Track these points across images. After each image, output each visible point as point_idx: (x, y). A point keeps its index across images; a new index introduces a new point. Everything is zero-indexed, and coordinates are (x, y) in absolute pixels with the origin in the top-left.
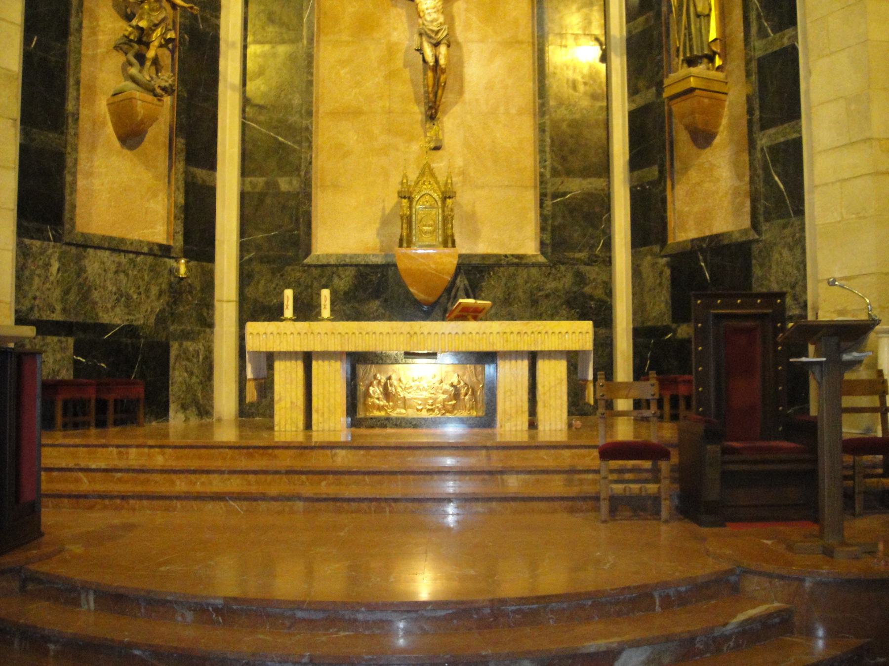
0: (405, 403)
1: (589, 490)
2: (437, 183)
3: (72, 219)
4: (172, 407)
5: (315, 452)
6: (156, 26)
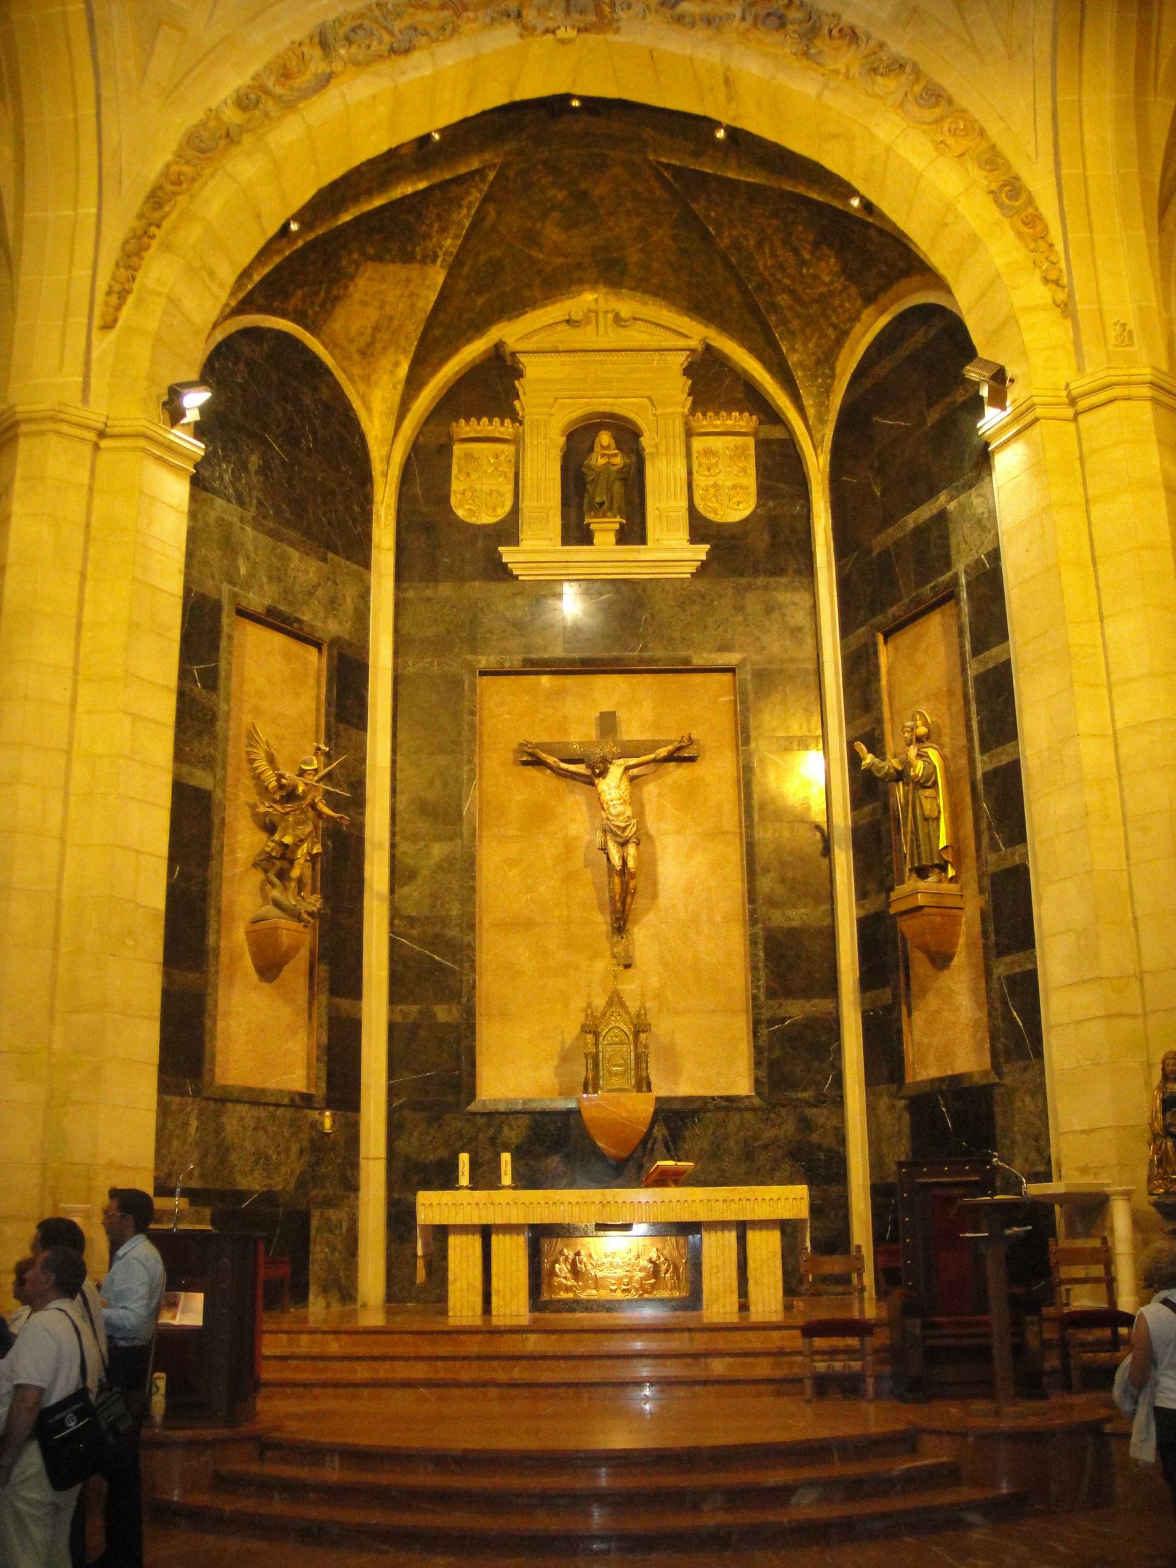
0: (597, 1283)
1: (797, 1371)
2: (628, 1013)
3: (212, 1071)
4: (313, 1289)
5: (506, 1336)
6: (302, 841)
